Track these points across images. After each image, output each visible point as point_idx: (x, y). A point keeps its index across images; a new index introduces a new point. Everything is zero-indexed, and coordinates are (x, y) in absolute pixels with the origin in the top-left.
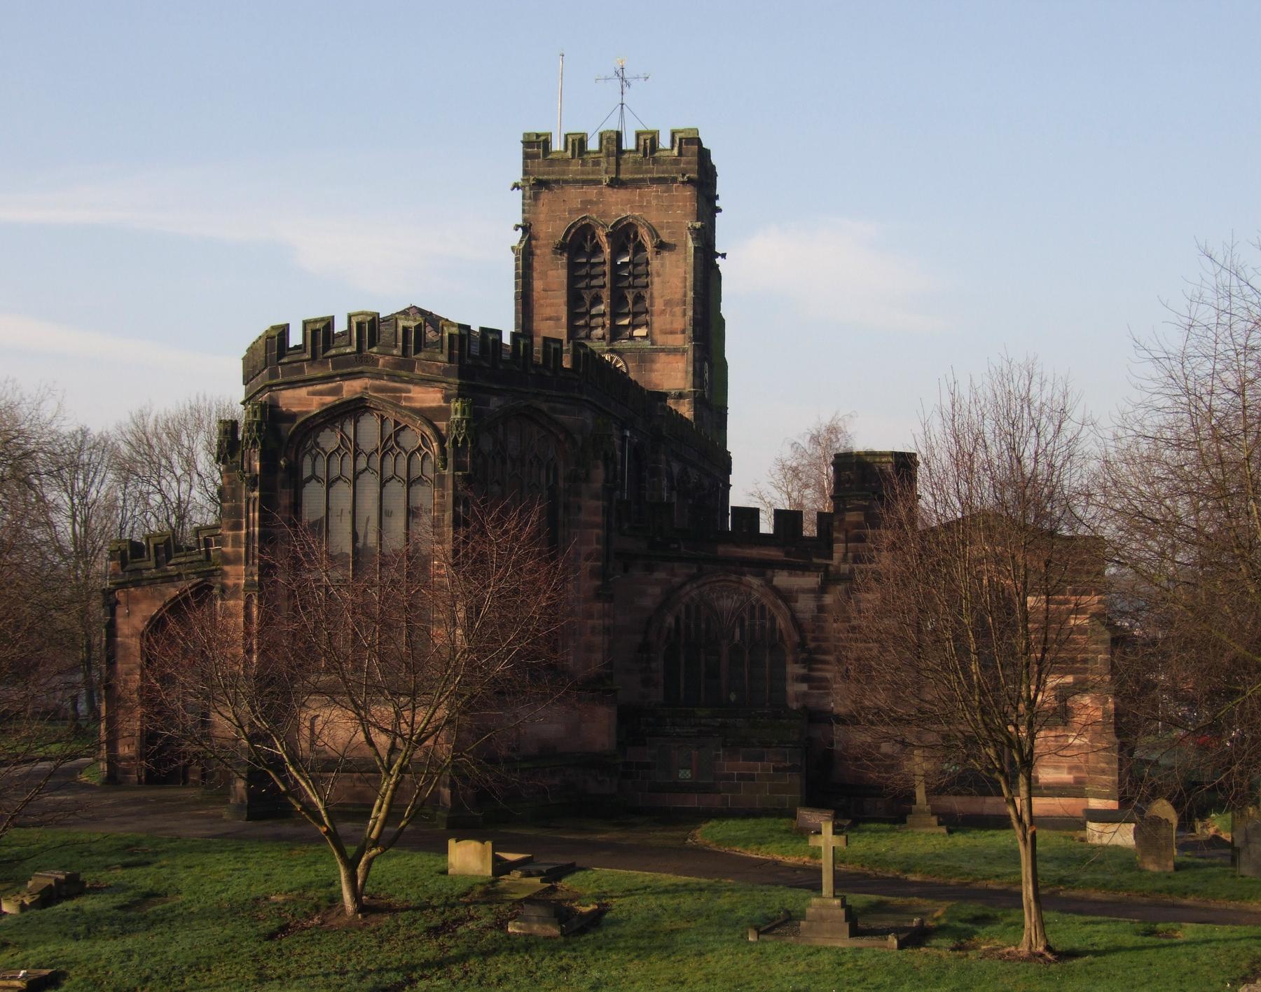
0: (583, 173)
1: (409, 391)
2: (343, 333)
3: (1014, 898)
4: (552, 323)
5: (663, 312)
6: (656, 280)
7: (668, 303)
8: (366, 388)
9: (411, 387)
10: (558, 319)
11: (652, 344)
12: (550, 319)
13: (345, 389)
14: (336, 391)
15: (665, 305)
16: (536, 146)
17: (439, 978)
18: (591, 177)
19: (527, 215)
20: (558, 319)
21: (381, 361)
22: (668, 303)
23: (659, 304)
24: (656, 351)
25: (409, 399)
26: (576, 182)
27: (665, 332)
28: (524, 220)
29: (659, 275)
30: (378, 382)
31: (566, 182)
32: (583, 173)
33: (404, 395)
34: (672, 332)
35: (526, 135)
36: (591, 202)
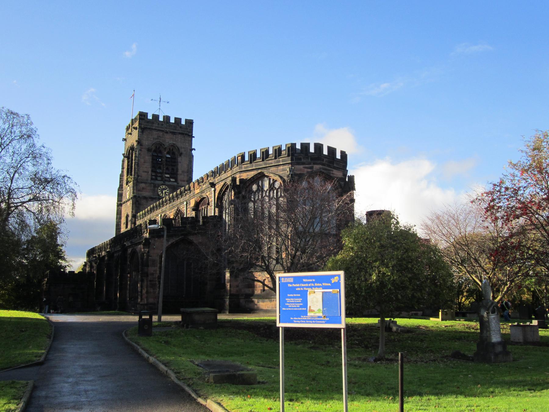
0: (158, 127)
1: (333, 171)
2: (284, 150)
3: (275, 311)
5: (181, 174)
6: (179, 164)
7: (183, 172)
8: (320, 168)
9: (333, 170)
10: (148, 172)
12: (146, 172)
13: (314, 168)
14: (312, 168)
15: (182, 172)
16: (142, 116)
17: (187, 366)
18: (160, 129)
19: (139, 137)
21: (325, 160)
22: (183, 172)
23: (180, 172)
24: (178, 186)
25: (333, 174)
26: (155, 129)
27: (181, 181)
28: (138, 139)
29: (180, 163)
30: (324, 167)
31: (152, 129)
32: (158, 127)
33: (331, 172)
34: (184, 181)
35: (140, 112)
36: (160, 137)
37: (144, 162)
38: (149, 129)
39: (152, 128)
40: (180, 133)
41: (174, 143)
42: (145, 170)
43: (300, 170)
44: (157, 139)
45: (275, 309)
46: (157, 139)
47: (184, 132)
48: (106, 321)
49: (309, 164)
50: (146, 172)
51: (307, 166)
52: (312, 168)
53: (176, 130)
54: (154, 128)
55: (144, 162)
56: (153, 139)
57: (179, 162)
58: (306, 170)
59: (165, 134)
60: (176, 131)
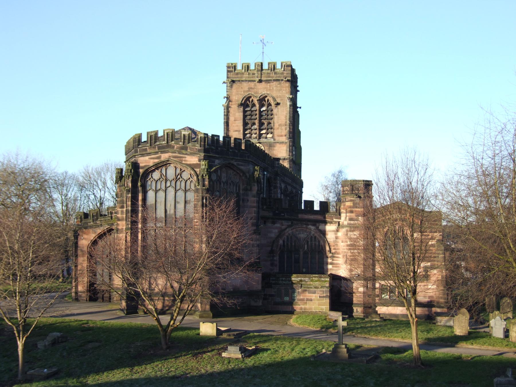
1: (185, 158)
2: (162, 137)
4: (237, 133)
5: (278, 128)
10: (239, 131)
11: (274, 140)
12: (237, 131)
20: (239, 131)
21: (175, 147)
22: (280, 125)
23: (276, 126)
24: (275, 143)
26: (246, 81)
27: (279, 136)
29: (276, 115)
31: (243, 81)
32: (249, 78)
33: (184, 159)
34: (281, 136)
36: (251, 88)
37: (235, 120)
38: (239, 81)
39: (242, 79)
40: (274, 80)
41: (268, 92)
42: (236, 128)
43: (146, 162)
44: (248, 91)
45: (344, 316)
46: (248, 91)
47: (279, 78)
48: (208, 335)
49: (156, 153)
50: (237, 131)
51: (153, 156)
52: (159, 158)
53: (269, 77)
54: (244, 79)
55: (235, 120)
56: (244, 92)
57: (275, 114)
58: (152, 161)
59: (258, 84)
60: (270, 79)
